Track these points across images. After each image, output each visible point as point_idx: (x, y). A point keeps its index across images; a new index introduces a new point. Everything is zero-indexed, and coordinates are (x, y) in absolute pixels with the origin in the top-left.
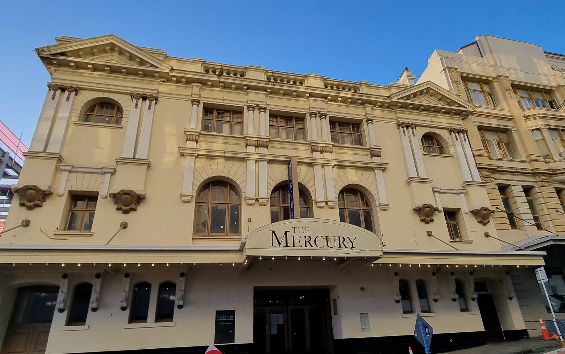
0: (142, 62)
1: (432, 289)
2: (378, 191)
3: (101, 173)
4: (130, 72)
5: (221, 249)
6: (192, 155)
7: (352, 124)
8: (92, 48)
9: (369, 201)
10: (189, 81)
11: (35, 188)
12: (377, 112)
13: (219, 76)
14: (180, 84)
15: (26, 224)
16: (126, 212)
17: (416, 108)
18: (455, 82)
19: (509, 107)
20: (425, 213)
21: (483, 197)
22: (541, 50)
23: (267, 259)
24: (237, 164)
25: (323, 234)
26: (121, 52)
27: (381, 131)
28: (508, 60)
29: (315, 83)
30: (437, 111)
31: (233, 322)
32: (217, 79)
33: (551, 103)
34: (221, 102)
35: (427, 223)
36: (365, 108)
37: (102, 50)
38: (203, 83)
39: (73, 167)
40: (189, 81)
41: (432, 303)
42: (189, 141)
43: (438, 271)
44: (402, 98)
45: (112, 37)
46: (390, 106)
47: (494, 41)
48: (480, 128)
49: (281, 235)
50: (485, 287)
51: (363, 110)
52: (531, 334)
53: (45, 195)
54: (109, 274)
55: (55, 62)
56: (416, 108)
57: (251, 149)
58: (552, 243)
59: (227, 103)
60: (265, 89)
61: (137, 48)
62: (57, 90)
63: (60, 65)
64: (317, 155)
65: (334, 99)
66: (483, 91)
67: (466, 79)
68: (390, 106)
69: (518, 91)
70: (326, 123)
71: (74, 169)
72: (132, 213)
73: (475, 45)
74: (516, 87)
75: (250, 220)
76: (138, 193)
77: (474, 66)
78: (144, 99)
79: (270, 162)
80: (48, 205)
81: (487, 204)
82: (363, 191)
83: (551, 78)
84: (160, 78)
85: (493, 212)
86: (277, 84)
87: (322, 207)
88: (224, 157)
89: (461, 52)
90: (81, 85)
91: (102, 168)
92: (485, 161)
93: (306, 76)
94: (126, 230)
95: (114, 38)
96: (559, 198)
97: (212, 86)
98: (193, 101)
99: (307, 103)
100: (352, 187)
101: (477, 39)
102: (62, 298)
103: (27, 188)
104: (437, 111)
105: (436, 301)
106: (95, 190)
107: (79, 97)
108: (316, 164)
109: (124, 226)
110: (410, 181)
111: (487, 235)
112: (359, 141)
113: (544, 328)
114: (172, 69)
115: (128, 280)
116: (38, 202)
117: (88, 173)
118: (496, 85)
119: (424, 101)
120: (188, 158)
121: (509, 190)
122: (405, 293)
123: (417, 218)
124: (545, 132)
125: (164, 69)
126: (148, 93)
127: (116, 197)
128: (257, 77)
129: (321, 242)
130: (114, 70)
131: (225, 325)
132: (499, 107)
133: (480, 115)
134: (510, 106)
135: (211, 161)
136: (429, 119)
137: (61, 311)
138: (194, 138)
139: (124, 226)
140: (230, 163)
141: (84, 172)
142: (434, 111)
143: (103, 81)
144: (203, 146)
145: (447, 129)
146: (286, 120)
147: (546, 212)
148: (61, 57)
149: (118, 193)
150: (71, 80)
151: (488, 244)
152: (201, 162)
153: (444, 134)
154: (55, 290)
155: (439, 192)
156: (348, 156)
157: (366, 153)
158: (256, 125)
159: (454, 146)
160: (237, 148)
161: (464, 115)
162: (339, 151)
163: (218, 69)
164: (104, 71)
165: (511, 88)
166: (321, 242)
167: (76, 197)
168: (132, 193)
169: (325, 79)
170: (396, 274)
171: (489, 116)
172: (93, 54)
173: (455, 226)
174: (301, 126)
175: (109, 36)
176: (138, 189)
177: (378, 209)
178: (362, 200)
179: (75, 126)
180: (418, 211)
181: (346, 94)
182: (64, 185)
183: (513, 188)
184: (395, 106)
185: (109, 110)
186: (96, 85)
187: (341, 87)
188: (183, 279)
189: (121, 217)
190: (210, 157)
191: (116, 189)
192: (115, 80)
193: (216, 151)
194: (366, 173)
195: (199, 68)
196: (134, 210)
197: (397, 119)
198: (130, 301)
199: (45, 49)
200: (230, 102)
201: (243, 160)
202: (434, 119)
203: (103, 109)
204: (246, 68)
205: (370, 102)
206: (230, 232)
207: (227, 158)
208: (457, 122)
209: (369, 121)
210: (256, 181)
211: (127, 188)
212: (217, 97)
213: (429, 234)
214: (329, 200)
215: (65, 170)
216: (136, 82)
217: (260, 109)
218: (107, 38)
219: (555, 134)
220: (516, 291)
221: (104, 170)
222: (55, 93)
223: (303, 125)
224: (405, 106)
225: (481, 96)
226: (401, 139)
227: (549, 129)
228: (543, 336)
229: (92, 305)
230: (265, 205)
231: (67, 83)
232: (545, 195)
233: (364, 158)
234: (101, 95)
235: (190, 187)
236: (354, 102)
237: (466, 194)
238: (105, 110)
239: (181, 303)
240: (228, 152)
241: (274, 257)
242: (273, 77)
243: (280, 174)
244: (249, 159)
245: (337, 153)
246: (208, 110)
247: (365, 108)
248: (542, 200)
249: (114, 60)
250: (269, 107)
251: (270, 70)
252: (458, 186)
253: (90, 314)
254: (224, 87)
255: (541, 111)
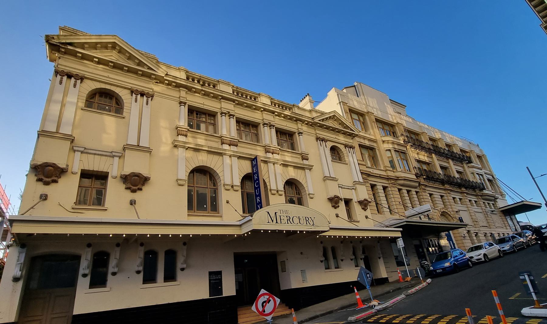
0: (140, 63)
1: (340, 253)
2: (224, 173)
3: (110, 156)
4: (130, 71)
5: (204, 225)
6: (184, 147)
7: (289, 134)
8: (97, 43)
9: (216, 181)
10: (178, 86)
11: (54, 166)
12: (304, 128)
13: (202, 85)
14: (170, 87)
15: (44, 197)
16: (134, 191)
17: (328, 128)
18: (346, 112)
19: (375, 134)
20: (334, 201)
21: (364, 193)
22: (388, 98)
23: (266, 231)
24: (216, 157)
25: (276, 215)
26: (121, 51)
27: (306, 142)
28: (372, 103)
29: (264, 100)
30: (339, 131)
31: (221, 280)
32: (200, 88)
33: (393, 133)
34: (201, 106)
35: (335, 208)
36: (297, 124)
37: (105, 46)
38: (189, 89)
39: (85, 148)
40: (178, 86)
41: (340, 263)
42: (181, 135)
43: (344, 241)
44: (320, 120)
45: (115, 37)
46: (312, 124)
47: (366, 88)
48: (361, 146)
49: (273, 215)
50: (367, 250)
51: (178, 93)
52: (390, 280)
53: (62, 172)
54: (126, 243)
55: (63, 50)
56: (328, 128)
57: (226, 147)
58: (405, 223)
59: (206, 107)
60: (233, 101)
61: (137, 50)
62: (78, 79)
63: (65, 53)
64: (270, 155)
65: (279, 115)
66: (359, 120)
67: (352, 111)
68: (312, 124)
69: (378, 123)
70: (233, 121)
71: (86, 151)
72: (53, 185)
73: (354, 88)
74: (378, 121)
75: (228, 202)
76: (145, 176)
77: (356, 103)
78: (142, 95)
79: (240, 158)
80: (63, 181)
81: (367, 197)
82: (212, 172)
83: (394, 117)
84: (155, 79)
85: (370, 202)
86: (242, 98)
87: (229, 190)
88: (207, 151)
89: (345, 91)
90: (87, 75)
91: (112, 152)
92: (364, 168)
93: (259, 95)
94: (46, 202)
95: (117, 38)
96: (372, 191)
97: (195, 92)
98: (181, 103)
99: (261, 115)
100: (206, 169)
101: (356, 84)
102: (85, 266)
103: (46, 165)
104: (339, 131)
105: (342, 260)
106: (105, 170)
107: (84, 84)
108: (270, 162)
109: (133, 203)
110: (325, 178)
111: (367, 217)
112: (293, 147)
113: (400, 275)
114: (167, 74)
115: (90, 250)
116: (56, 178)
117: (98, 155)
118: (367, 117)
119: (330, 123)
120: (181, 150)
121: (375, 188)
122: (325, 255)
123: (329, 205)
124: (393, 152)
125: (161, 73)
126: (146, 90)
127: (125, 179)
128: (226, 89)
129: (296, 220)
130: (117, 67)
131: (215, 283)
132: (369, 133)
133: (360, 137)
134: (375, 133)
135: (197, 153)
136: (334, 136)
137: (85, 276)
138: (185, 133)
139: (133, 203)
140: (211, 156)
141: (95, 154)
142: (337, 132)
143: (106, 74)
144: (190, 140)
145: (344, 144)
146: (245, 126)
147: (394, 203)
148: (70, 47)
149: (128, 175)
150: (77, 69)
151: (369, 223)
152: (190, 154)
153: (342, 147)
154: (78, 258)
155: (342, 188)
156: (288, 157)
157: (299, 157)
158: (227, 128)
159: (348, 156)
160: (215, 144)
161: (352, 136)
162: (283, 153)
163: (197, 78)
164: (108, 65)
165: (348, 111)
166: (296, 220)
167: (85, 174)
168: (141, 176)
169: (272, 99)
170: (322, 243)
171: (364, 138)
172: (96, 49)
173: (348, 210)
174: (255, 132)
175: (112, 36)
176: (145, 173)
177: (223, 188)
178: (211, 179)
179: (82, 111)
180: (331, 200)
181: (287, 113)
182: (79, 163)
183: (378, 187)
184: (315, 125)
185: (108, 100)
186: (101, 76)
187: (284, 107)
188: (118, 249)
189: (130, 196)
190: (196, 150)
191: (127, 171)
192: (116, 75)
193: (202, 146)
194: (300, 171)
195: (183, 76)
196: (141, 189)
197: (220, 109)
198: (91, 268)
199: (55, 37)
200: (103, 78)
201: (221, 154)
202: (337, 137)
203: (104, 99)
204: (218, 82)
205: (300, 120)
206: (211, 211)
207: (209, 152)
208: (349, 141)
209: (300, 133)
210: (231, 172)
211: (137, 170)
212: (198, 101)
213: (337, 216)
214: (234, 184)
215: (78, 151)
216: (135, 80)
217: (230, 115)
218: (111, 37)
219: (397, 153)
220: (382, 253)
221: (114, 154)
222: (62, 78)
223: (214, 120)
224: (321, 126)
225: (358, 123)
226: (319, 148)
227: (395, 151)
228: (399, 280)
229: (111, 270)
230: (182, 185)
231: (74, 71)
232: (394, 192)
233: (298, 160)
234: (103, 86)
235: (183, 174)
236: (291, 119)
237: (355, 189)
238: (103, 99)
239: (116, 270)
240: (211, 147)
241: (250, 231)
242: (237, 92)
243: (247, 168)
244: (225, 154)
245: (281, 155)
246: (192, 111)
247: (297, 124)
248: (392, 196)
249: (112, 56)
250: (189, 103)
251: (235, 85)
252: (350, 184)
253: (110, 277)
254: (204, 95)
255: (390, 138)
